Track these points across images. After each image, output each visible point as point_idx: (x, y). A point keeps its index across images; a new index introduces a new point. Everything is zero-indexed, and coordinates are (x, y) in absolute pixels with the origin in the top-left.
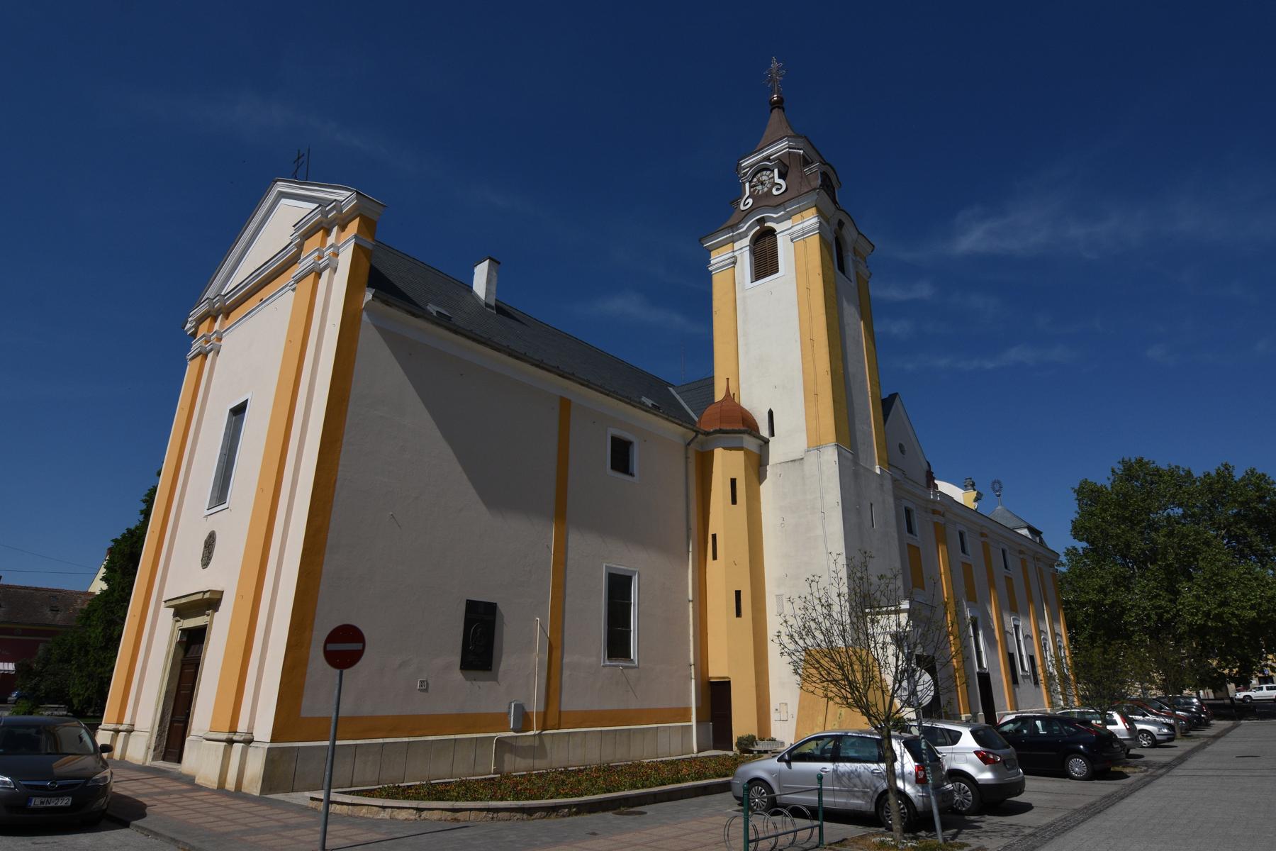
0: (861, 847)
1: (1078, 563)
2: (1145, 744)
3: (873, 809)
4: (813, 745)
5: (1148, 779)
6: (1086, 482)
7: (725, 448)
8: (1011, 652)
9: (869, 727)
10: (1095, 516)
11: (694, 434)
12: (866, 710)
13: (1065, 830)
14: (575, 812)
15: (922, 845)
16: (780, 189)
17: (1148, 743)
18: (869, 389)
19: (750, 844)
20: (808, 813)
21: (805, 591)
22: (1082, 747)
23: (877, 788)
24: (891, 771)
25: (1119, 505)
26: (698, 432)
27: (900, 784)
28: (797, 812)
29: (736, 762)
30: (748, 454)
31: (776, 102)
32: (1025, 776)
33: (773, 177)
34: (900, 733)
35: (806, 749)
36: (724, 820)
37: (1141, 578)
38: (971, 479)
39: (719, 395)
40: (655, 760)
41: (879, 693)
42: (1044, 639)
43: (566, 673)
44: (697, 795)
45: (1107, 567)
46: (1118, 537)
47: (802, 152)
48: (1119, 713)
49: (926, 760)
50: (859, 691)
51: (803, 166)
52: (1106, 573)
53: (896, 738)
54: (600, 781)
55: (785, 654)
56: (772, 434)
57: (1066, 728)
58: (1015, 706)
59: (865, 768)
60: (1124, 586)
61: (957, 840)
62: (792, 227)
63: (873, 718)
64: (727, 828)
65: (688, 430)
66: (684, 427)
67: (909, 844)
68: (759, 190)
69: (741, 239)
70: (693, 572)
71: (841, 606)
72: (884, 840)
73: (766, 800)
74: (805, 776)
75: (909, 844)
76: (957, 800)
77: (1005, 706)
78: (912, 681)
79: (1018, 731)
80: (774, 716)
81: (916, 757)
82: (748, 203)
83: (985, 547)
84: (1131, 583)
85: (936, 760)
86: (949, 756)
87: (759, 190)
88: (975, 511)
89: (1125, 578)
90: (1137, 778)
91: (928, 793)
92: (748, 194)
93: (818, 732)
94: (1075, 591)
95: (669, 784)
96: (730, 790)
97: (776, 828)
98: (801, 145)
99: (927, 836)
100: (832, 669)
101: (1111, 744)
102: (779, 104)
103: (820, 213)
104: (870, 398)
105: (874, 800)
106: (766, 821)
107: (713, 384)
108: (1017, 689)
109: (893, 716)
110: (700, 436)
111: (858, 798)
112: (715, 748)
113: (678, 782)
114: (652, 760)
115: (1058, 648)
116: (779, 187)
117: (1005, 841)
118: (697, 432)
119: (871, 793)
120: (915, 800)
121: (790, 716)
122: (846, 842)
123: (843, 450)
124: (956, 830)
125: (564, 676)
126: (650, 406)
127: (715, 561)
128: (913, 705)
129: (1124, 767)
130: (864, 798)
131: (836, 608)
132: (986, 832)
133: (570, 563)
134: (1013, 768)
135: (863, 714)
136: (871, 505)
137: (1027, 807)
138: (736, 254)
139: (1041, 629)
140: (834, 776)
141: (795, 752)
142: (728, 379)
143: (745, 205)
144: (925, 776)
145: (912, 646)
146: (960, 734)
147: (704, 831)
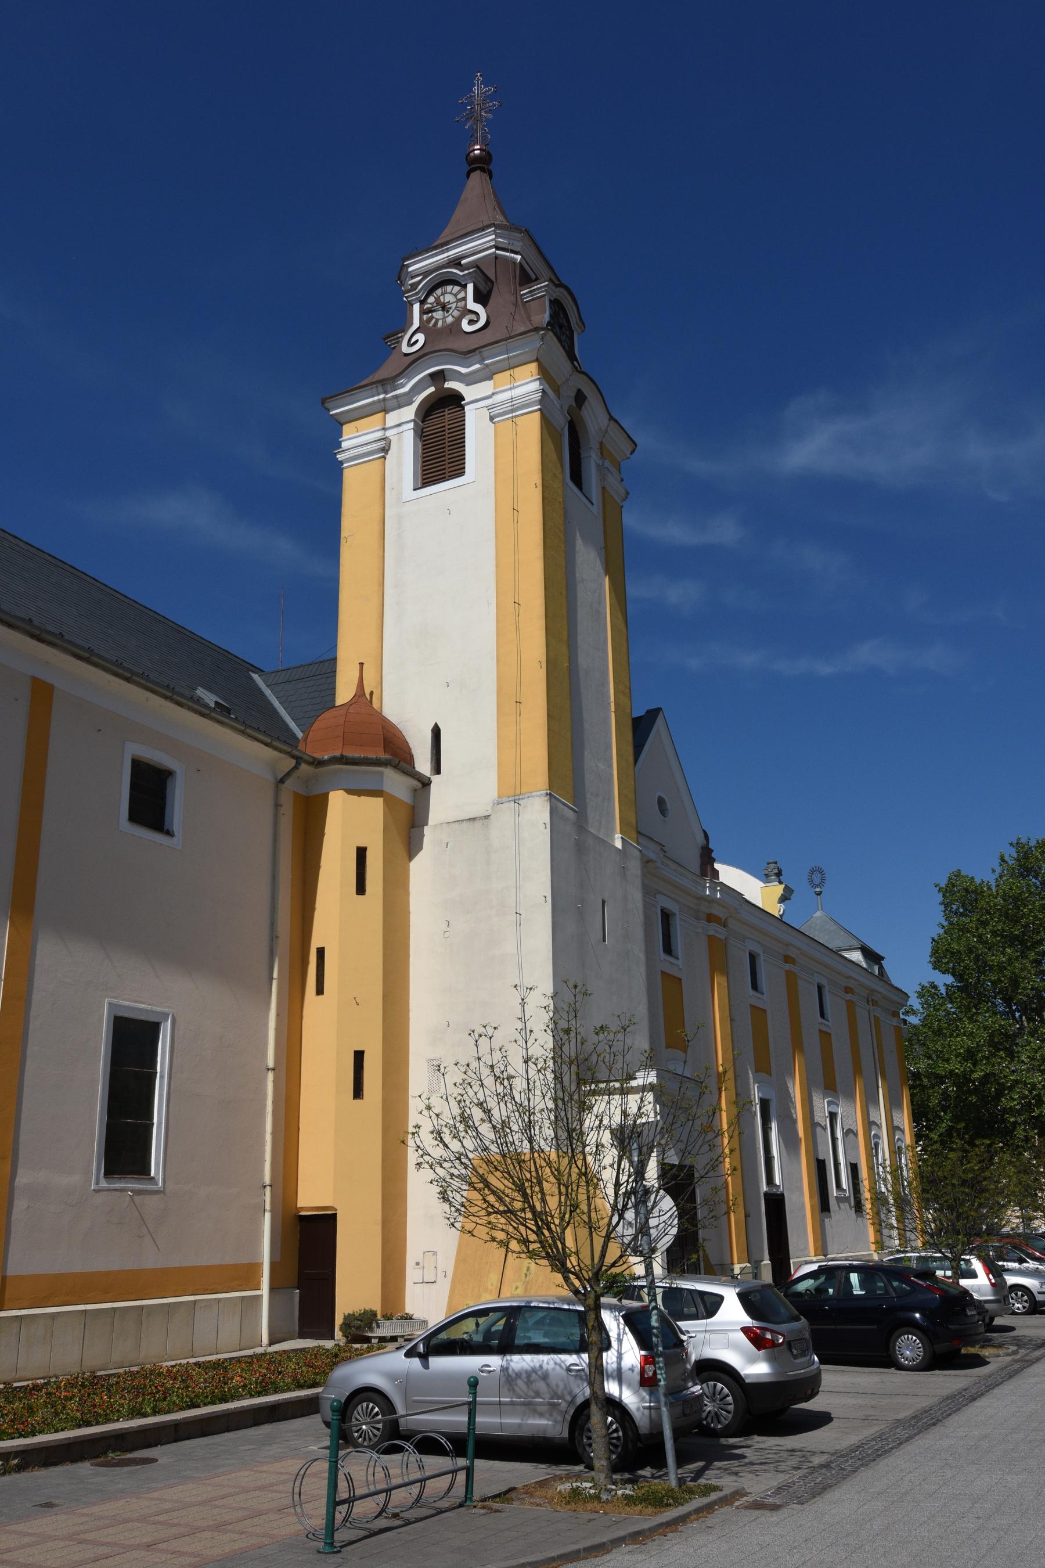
0: (538, 1500)
1: (938, 1010)
2: (1018, 1309)
3: (565, 1434)
4: (469, 1325)
5: (1017, 1366)
6: (958, 874)
7: (350, 792)
8: (821, 1158)
9: (566, 1293)
10: (968, 931)
11: (293, 763)
12: (559, 1262)
13: (879, 1455)
14: (17, 1465)
15: (640, 1493)
16: (477, 321)
17: (1024, 1307)
18: (612, 699)
19: (339, 1508)
20: (449, 1446)
21: (467, 1054)
22: (917, 1315)
23: (574, 1397)
24: (596, 1368)
25: (1007, 915)
26: (301, 758)
27: (612, 1388)
28: (428, 1445)
29: (337, 1358)
30: (391, 803)
31: (477, 159)
32: (823, 1367)
33: (464, 299)
34: (620, 1300)
35: (458, 1333)
36: (294, 1465)
37: (1033, 1036)
38: (776, 863)
39: (344, 694)
40: (184, 1362)
41: (584, 1232)
42: (876, 1136)
43: (20, 1205)
44: (257, 1423)
45: (980, 1018)
46: (1001, 968)
47: (519, 257)
48: (979, 1258)
49: (657, 1346)
50: (549, 1229)
51: (521, 285)
52: (979, 1028)
53: (611, 1308)
54: (72, 1405)
55: (426, 1166)
56: (437, 769)
57: (895, 1284)
58: (822, 1249)
59: (556, 1363)
60: (1005, 1049)
61: (702, 1481)
62: (493, 394)
63: (572, 1276)
64: (300, 1478)
65: (282, 755)
66: (275, 748)
67: (620, 1492)
68: (437, 320)
69: (400, 407)
70: (278, 1015)
71: (528, 1079)
72: (578, 1487)
73: (380, 1426)
74: (448, 1378)
75: (620, 1492)
76: (710, 1412)
77: (806, 1248)
78: (642, 1210)
79: (820, 1290)
80: (412, 1275)
81: (643, 1342)
82: (417, 341)
83: (790, 977)
84: (1017, 1045)
85: (676, 1344)
86: (700, 1336)
87: (437, 320)
88: (780, 920)
89: (1007, 1036)
90: (999, 1365)
91: (658, 1401)
92: (416, 324)
93: (487, 1300)
94: (929, 1057)
95: (205, 1405)
96: (317, 1411)
97: (388, 1476)
98: (518, 246)
99: (653, 1477)
100: (507, 1191)
101: (964, 1311)
102: (482, 164)
103: (545, 375)
104: (613, 714)
105: (569, 1418)
106: (372, 1463)
107: (333, 672)
108: (827, 1221)
109: (606, 1271)
110: (304, 767)
111: (541, 1415)
112: (302, 1335)
113: (224, 1400)
114: (178, 1362)
115: (896, 1151)
116: (473, 317)
117: (781, 1479)
118: (299, 760)
119: (564, 1405)
120: (637, 1416)
121: (440, 1275)
122: (513, 1495)
123: (560, 806)
124: (701, 1464)
125: (15, 1210)
126: (213, 705)
127: (320, 997)
128: (641, 1252)
129: (982, 1347)
130: (551, 1415)
131: (519, 1084)
132: (752, 1464)
133: (37, 996)
134: (803, 1354)
135: (554, 1268)
136: (604, 902)
137: (822, 1419)
138: (389, 433)
139: (872, 1119)
140: (503, 1379)
141: (443, 1336)
142: (362, 664)
143: (410, 344)
144: (655, 1373)
145: (645, 1149)
146: (719, 1299)
147: (261, 1488)
